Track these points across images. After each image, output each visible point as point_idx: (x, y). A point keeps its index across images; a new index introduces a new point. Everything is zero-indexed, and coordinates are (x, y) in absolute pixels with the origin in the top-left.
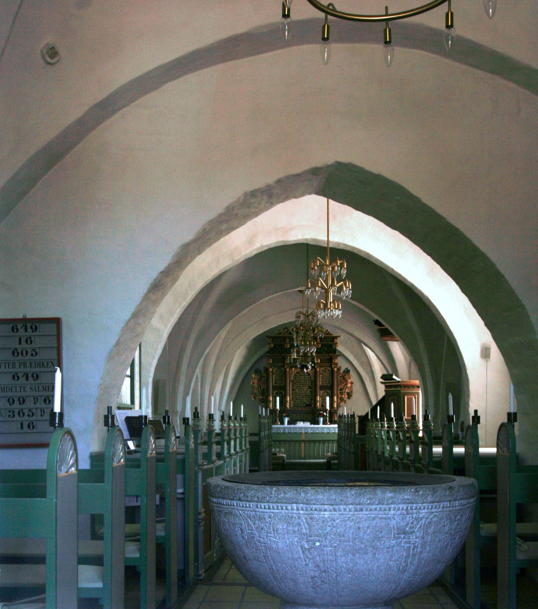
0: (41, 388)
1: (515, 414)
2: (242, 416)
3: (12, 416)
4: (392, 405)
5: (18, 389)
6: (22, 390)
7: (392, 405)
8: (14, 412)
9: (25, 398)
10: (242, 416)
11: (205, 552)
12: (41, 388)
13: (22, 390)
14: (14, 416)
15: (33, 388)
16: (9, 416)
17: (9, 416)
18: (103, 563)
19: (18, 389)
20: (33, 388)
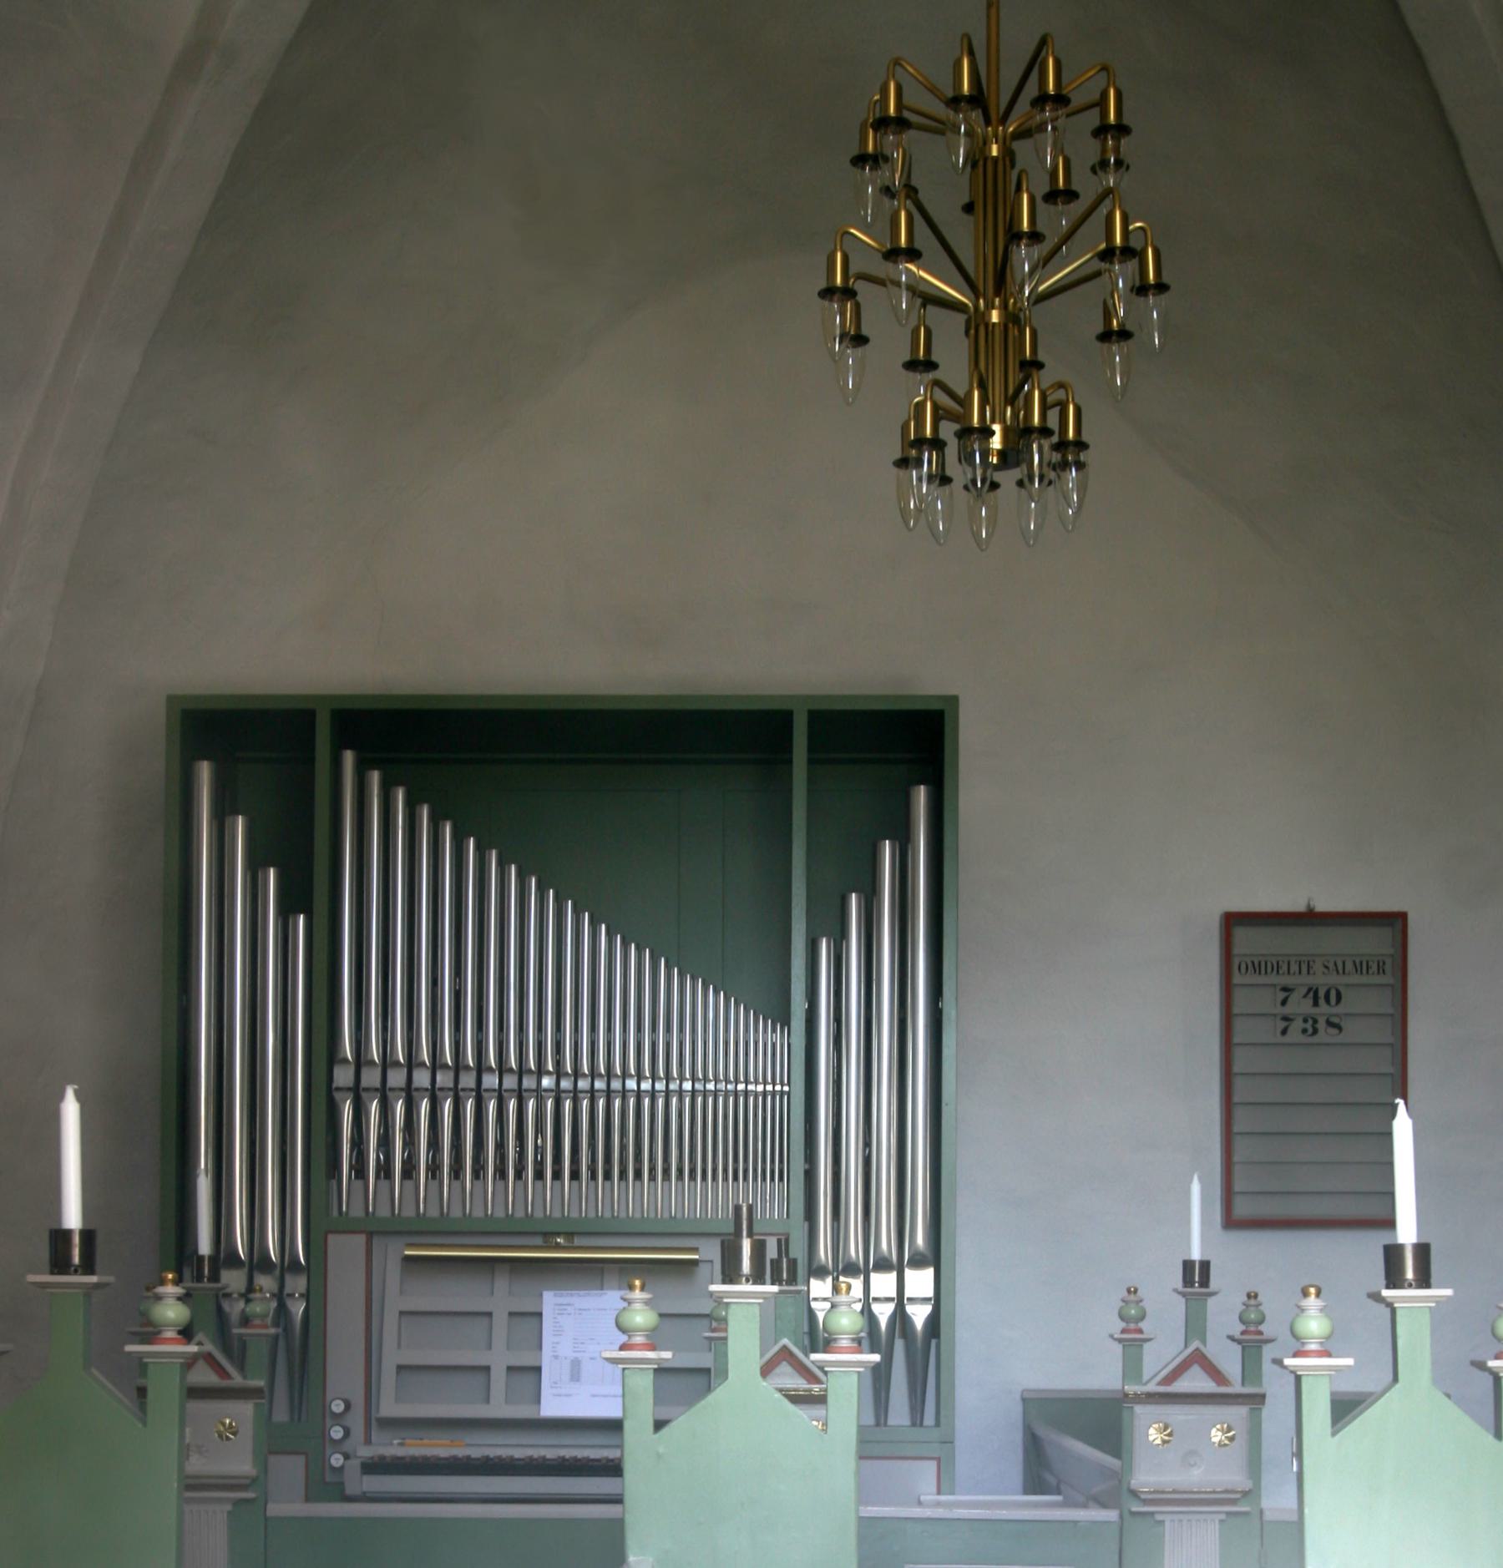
0: (1349, 966)
1: (1205, 1266)
2: (72, 1217)
3: (1310, 1031)
4: (71, 1111)
5: (1294, 968)
6: (1304, 969)
7: (71, 1111)
8: (1315, 1021)
9: (1342, 990)
10: (72, 1217)
11: (1159, 1384)
12: (1349, 966)
13: (1304, 969)
14: (1315, 1031)
15: (1331, 965)
16: (1304, 1031)
17: (1304, 1031)
18: (862, 1539)
19: (1294, 968)
20: (1331, 965)
